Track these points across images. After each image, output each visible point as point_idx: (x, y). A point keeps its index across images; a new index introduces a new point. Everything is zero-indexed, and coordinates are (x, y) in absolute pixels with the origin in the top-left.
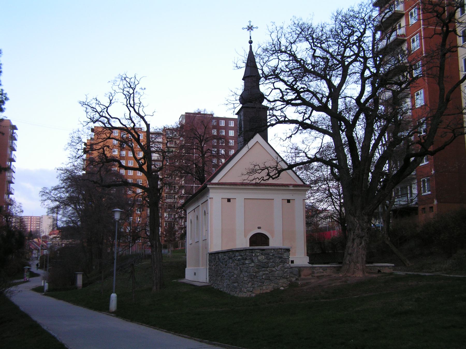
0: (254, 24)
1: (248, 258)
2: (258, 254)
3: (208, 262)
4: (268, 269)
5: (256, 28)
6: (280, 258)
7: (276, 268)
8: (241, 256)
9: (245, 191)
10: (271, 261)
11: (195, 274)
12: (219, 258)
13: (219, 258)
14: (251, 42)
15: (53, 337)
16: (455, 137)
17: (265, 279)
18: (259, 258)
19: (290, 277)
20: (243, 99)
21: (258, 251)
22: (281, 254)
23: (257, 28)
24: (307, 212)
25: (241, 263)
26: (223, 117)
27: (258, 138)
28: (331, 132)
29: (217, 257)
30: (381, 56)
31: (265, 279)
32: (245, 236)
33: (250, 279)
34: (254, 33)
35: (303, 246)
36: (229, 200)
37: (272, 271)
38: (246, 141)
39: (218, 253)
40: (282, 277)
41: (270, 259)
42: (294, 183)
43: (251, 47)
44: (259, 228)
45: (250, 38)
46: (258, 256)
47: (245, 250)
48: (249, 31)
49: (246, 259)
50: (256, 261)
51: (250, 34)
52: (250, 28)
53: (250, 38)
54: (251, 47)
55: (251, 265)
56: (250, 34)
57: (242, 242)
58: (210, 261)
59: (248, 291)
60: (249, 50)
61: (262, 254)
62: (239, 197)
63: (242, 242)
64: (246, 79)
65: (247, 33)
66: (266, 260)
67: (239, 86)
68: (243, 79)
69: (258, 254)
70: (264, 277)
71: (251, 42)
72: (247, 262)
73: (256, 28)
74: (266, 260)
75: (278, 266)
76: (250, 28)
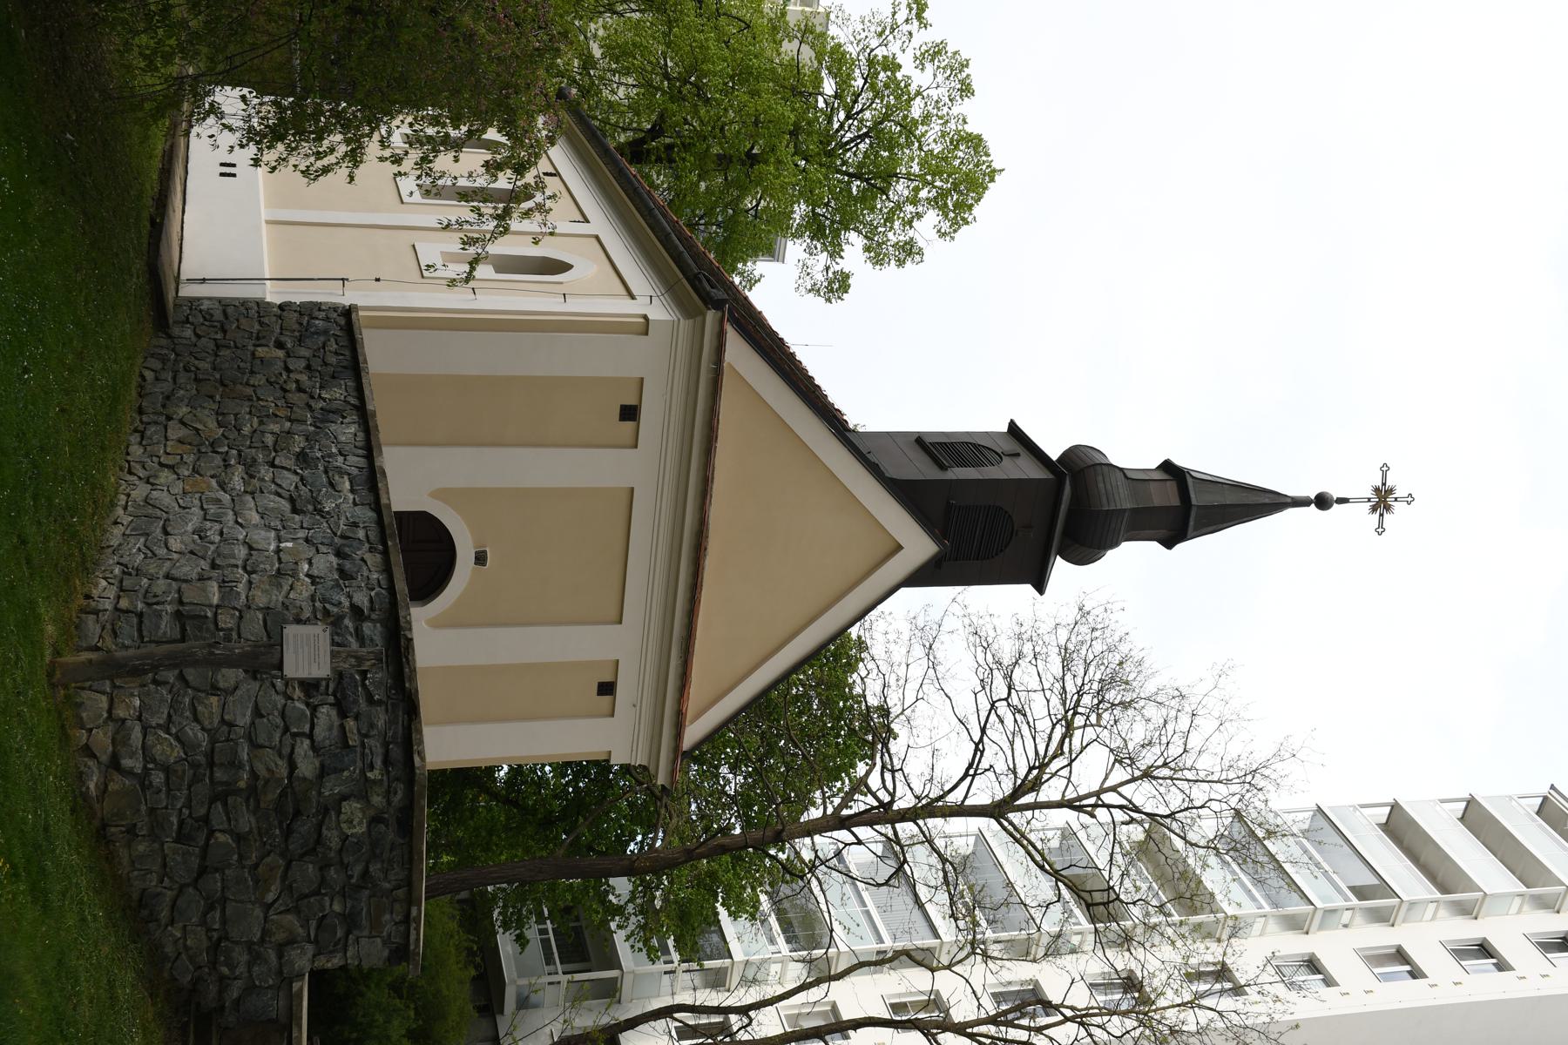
0: (1399, 515)
2: (377, 800)
5: (1381, 524)
6: (351, 921)
14: (1323, 502)
18: (352, 808)
19: (222, 978)
20: (1080, 467)
21: (397, 798)
24: (596, 763)
26: (486, 450)
27: (919, 546)
34: (1359, 516)
35: (454, 758)
38: (906, 493)
39: (355, 367)
44: (480, 559)
46: (364, 797)
48: (1369, 493)
51: (1359, 500)
56: (1359, 500)
57: (412, 483)
61: (375, 820)
62: (641, 469)
65: (1364, 488)
67: (1133, 451)
68: (1167, 466)
69: (377, 800)
71: (1323, 502)
72: (327, 714)
73: (1381, 524)
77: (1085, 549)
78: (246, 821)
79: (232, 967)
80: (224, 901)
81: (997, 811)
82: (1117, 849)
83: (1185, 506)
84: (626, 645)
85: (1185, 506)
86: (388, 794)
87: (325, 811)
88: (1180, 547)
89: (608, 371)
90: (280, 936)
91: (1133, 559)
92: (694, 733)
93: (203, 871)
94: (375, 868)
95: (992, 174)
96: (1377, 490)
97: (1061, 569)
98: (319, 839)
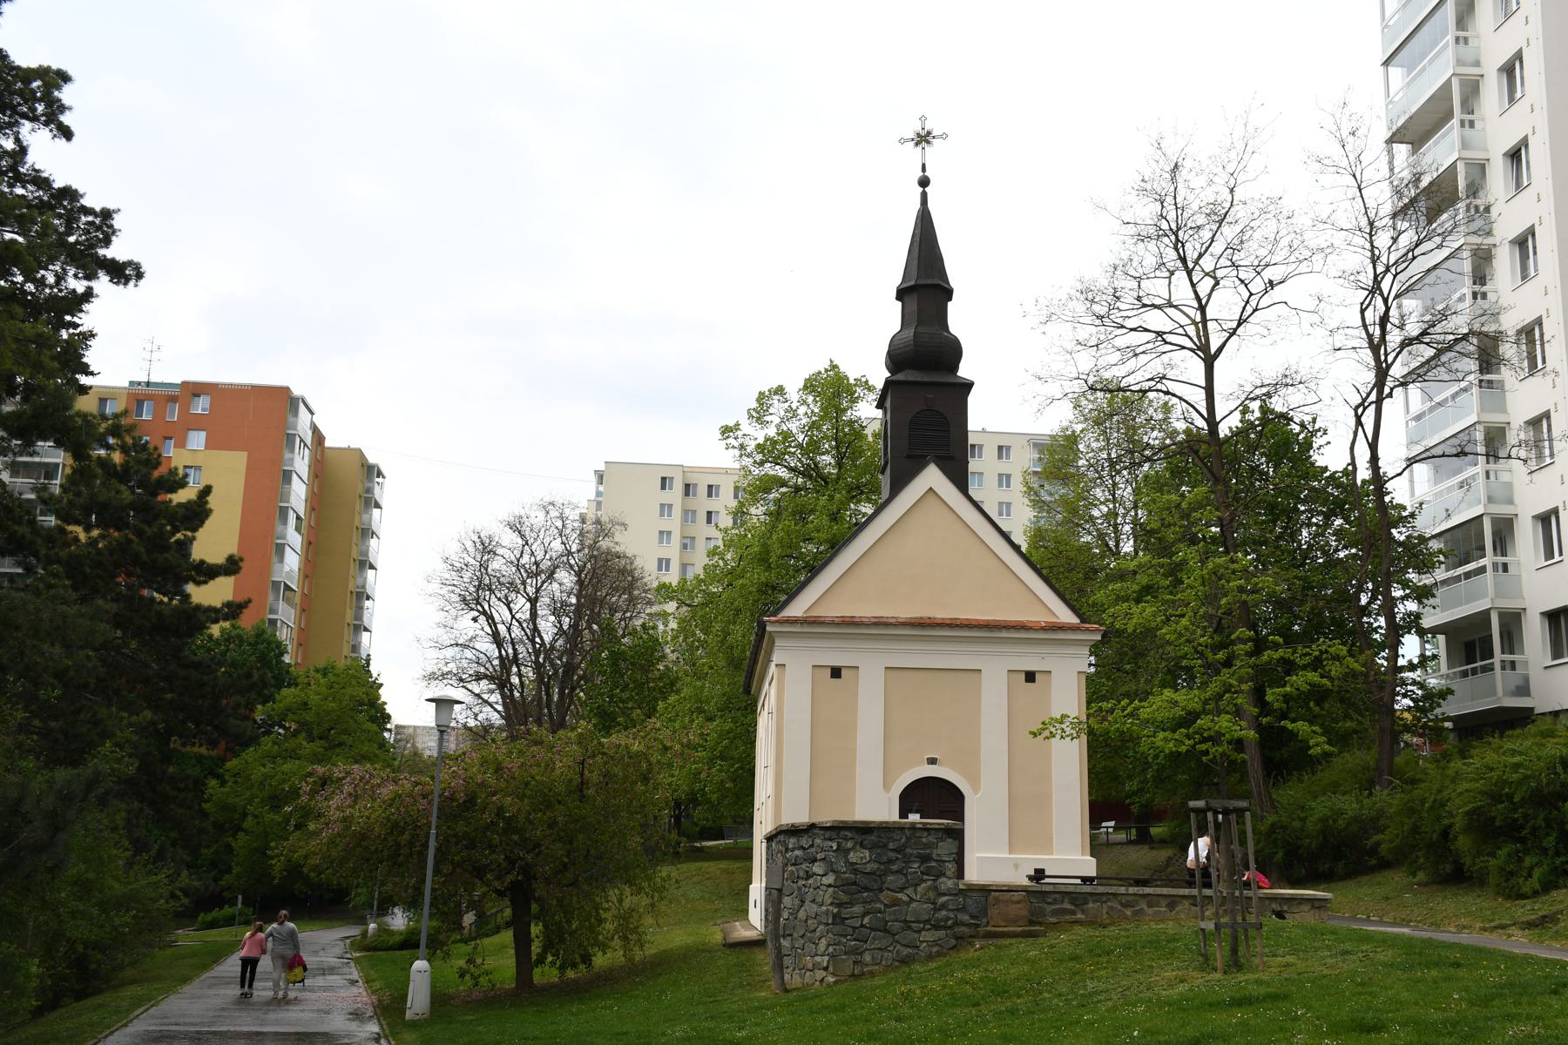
1: (819, 856)
4: (881, 896)
5: (940, 137)
6: (925, 859)
7: (910, 891)
8: (802, 848)
9: (834, 643)
10: (894, 867)
14: (924, 182)
16: (1217, 283)
17: (872, 929)
18: (853, 857)
21: (849, 834)
22: (929, 846)
23: (944, 136)
25: (802, 874)
27: (932, 477)
31: (872, 929)
32: (887, 786)
34: (934, 152)
36: (836, 672)
37: (896, 902)
40: (927, 922)
41: (890, 861)
42: (1041, 618)
43: (924, 196)
44: (932, 761)
45: (924, 169)
46: (848, 851)
47: (883, 829)
49: (814, 860)
51: (923, 156)
52: (923, 139)
53: (924, 169)
54: (924, 196)
55: (826, 881)
56: (923, 156)
59: (816, 966)
60: (918, 206)
61: (862, 846)
62: (871, 665)
63: (876, 803)
64: (906, 299)
65: (913, 154)
66: (876, 866)
69: (850, 845)
70: (866, 920)
71: (924, 182)
73: (940, 137)
74: (876, 866)
76: (923, 139)
77: (952, 352)
78: (858, 909)
79: (948, 919)
80: (905, 921)
81: (1209, 361)
82: (1292, 259)
83: (925, 287)
84: (995, 669)
85: (925, 287)
86: (846, 839)
87: (855, 871)
88: (953, 283)
89: (808, 688)
90: (931, 894)
91: (959, 318)
92: (1066, 616)
93: (886, 931)
94: (891, 846)
95: (834, 367)
96: (929, 133)
97: (964, 371)
98: (872, 873)
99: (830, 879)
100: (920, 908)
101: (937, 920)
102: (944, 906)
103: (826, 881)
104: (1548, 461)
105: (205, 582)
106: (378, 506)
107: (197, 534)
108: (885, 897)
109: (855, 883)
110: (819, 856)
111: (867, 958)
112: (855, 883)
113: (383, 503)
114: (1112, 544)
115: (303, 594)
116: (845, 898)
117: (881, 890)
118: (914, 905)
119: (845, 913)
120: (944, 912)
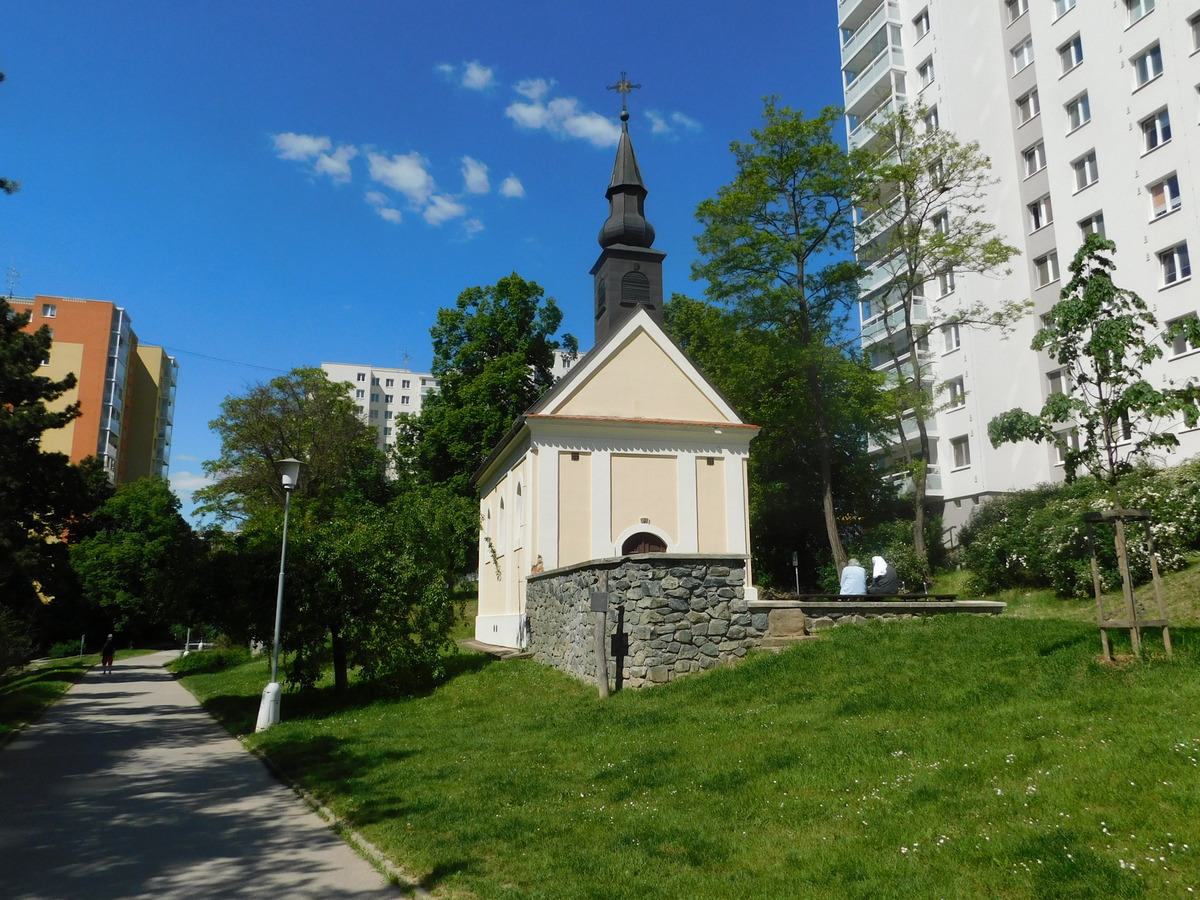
1: (633, 585)
3: (524, 600)
5: (636, 87)
7: (710, 610)
11: (495, 629)
12: (551, 590)
13: (551, 590)
15: (1021, 191)
17: (682, 643)
28: (35, 583)
29: (547, 586)
30: (916, 845)
33: (639, 642)
40: (724, 635)
42: (723, 421)
44: (645, 521)
50: (655, 591)
55: (641, 604)
58: (530, 597)
73: (636, 87)
75: (713, 606)
78: (669, 627)
79: (740, 632)
87: (668, 596)
99: (647, 602)
100: (717, 625)
101: (732, 633)
102: (736, 622)
103: (641, 604)
104: (955, 348)
105: (56, 397)
106: (173, 385)
107: (42, 438)
108: (691, 616)
109: (667, 606)
110: (633, 585)
111: (678, 666)
112: (667, 606)
113: (177, 384)
114: (1098, 253)
115: (122, 439)
116: (660, 618)
117: (687, 611)
118: (713, 621)
119: (659, 629)
120: (736, 627)
